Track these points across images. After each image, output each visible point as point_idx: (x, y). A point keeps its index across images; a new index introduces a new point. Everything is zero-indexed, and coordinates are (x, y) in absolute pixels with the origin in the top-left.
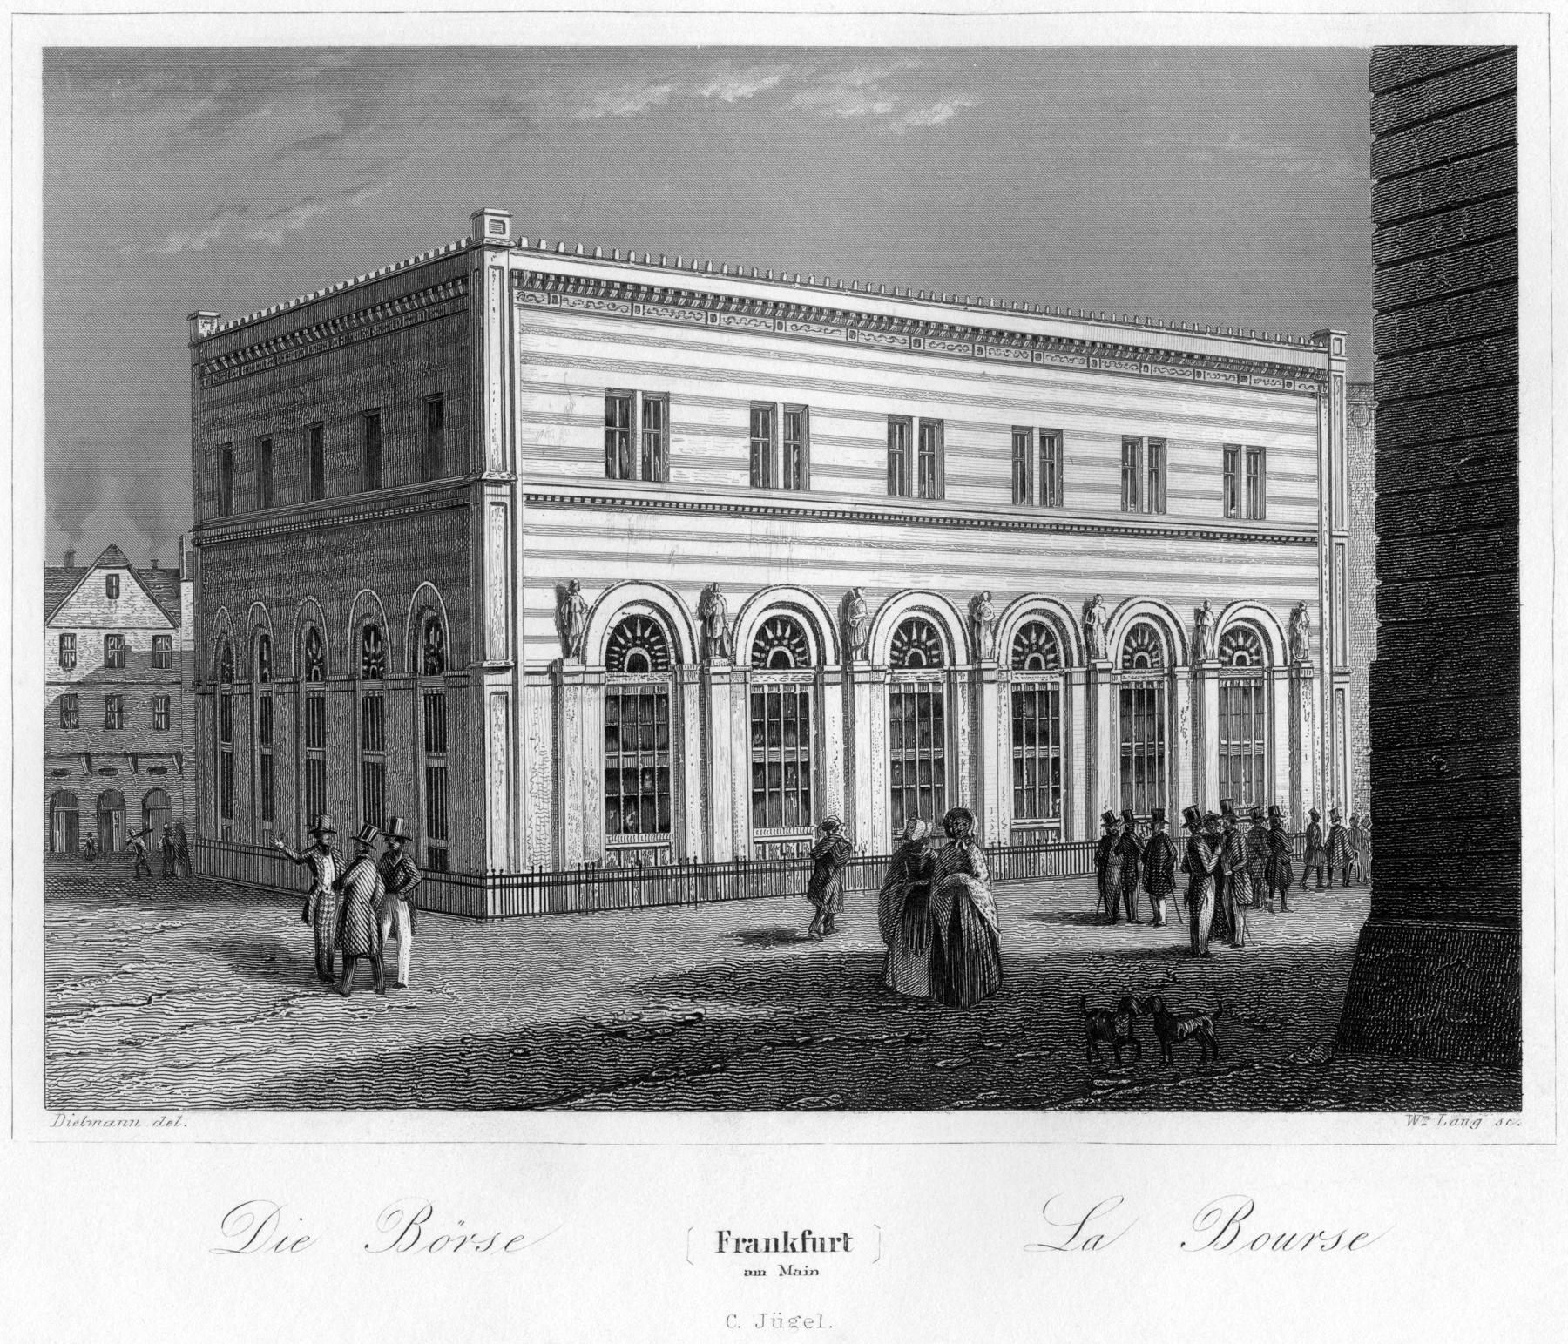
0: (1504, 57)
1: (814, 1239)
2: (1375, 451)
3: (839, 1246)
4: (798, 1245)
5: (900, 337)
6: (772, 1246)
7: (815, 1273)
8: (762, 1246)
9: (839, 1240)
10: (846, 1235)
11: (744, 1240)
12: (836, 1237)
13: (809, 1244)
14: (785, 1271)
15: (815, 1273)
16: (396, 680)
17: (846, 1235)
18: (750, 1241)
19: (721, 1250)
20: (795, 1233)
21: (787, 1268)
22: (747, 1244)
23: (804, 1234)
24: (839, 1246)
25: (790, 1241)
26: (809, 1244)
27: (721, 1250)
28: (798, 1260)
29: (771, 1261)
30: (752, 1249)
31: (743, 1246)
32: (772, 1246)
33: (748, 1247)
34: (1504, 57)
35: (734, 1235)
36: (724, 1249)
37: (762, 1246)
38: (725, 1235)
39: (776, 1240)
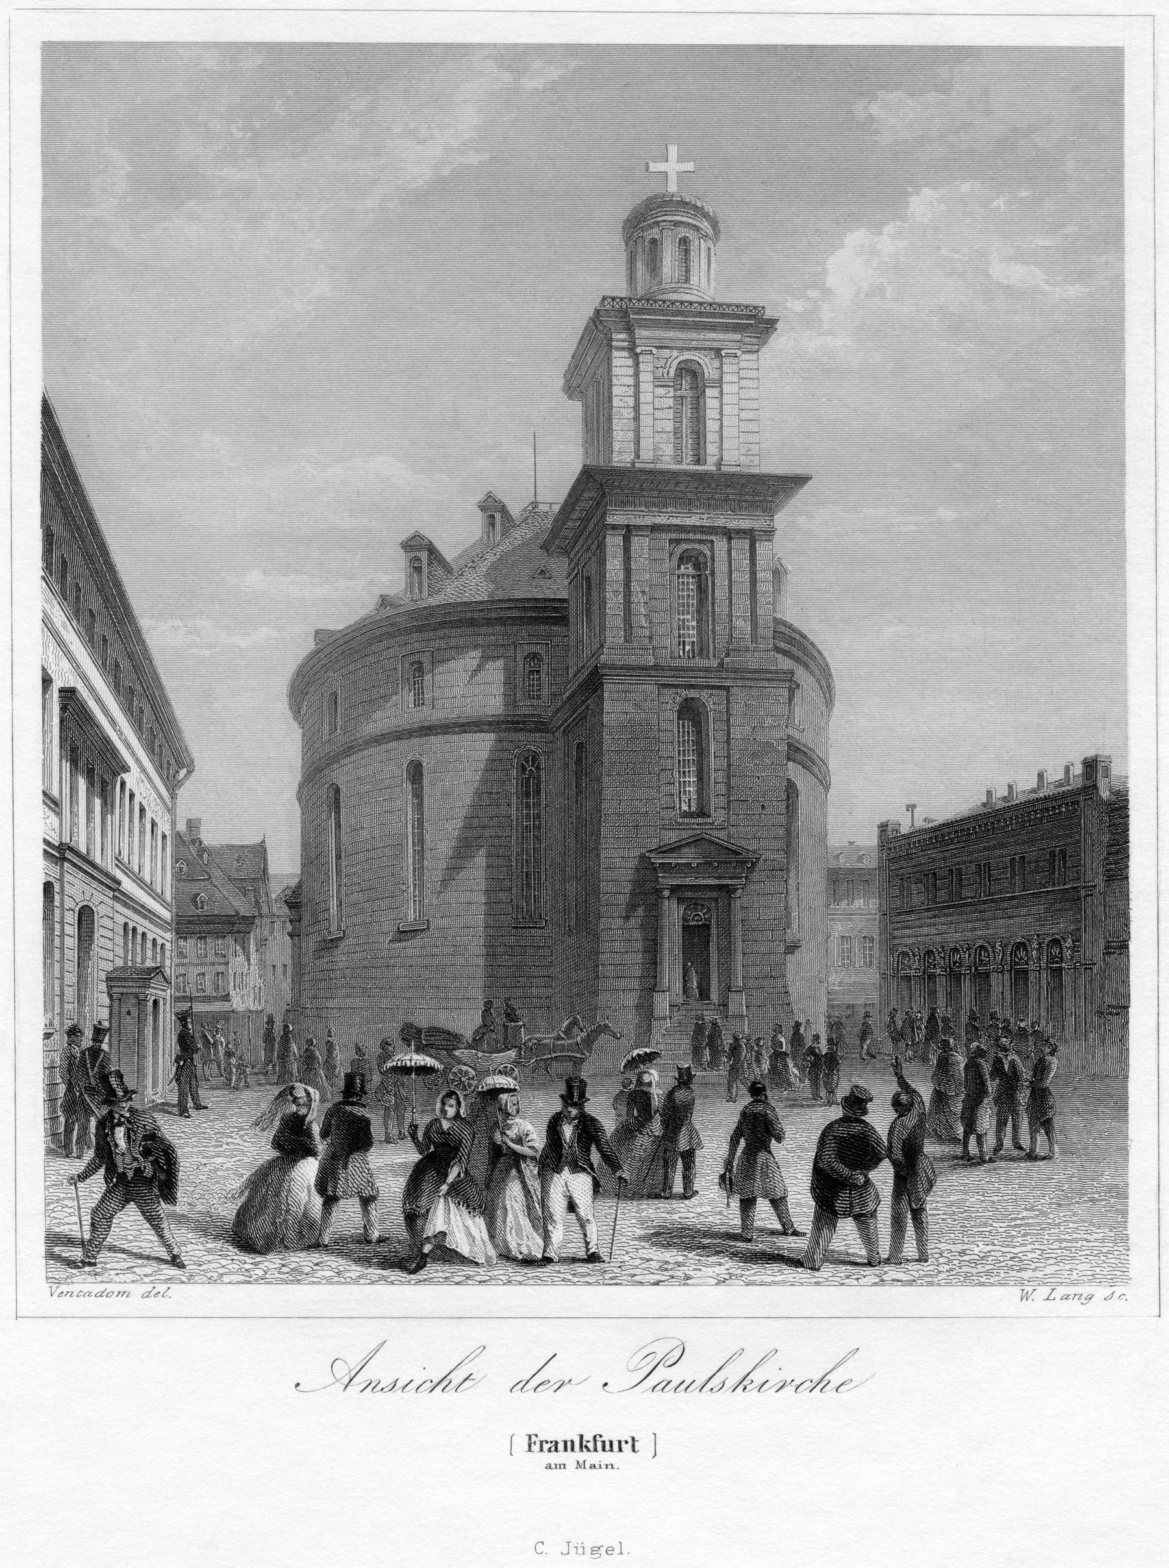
0: (1113, 58)
1: (604, 1442)
2: (413, 1076)
3: (627, 1448)
4: (591, 1445)
5: (128, 1160)
6: (569, 1446)
7: (609, 1467)
8: (561, 1446)
9: (627, 1442)
10: (633, 1439)
11: (547, 1442)
12: (623, 1439)
13: (599, 1445)
14: (580, 1465)
15: (609, 1467)
16: (637, 408)
17: (633, 1439)
18: (551, 1442)
19: (530, 1450)
20: (588, 1437)
21: (581, 1462)
22: (549, 1445)
23: (595, 1437)
24: (627, 1448)
25: (584, 1443)
26: (599, 1445)
27: (530, 1450)
28: (591, 1458)
29: (570, 1458)
30: (553, 1449)
31: (546, 1447)
32: (569, 1446)
33: (550, 1448)
34: (1113, 58)
35: (541, 1438)
36: (623, 1450)
37: (561, 1446)
38: (534, 1439)
39: (572, 1442)
